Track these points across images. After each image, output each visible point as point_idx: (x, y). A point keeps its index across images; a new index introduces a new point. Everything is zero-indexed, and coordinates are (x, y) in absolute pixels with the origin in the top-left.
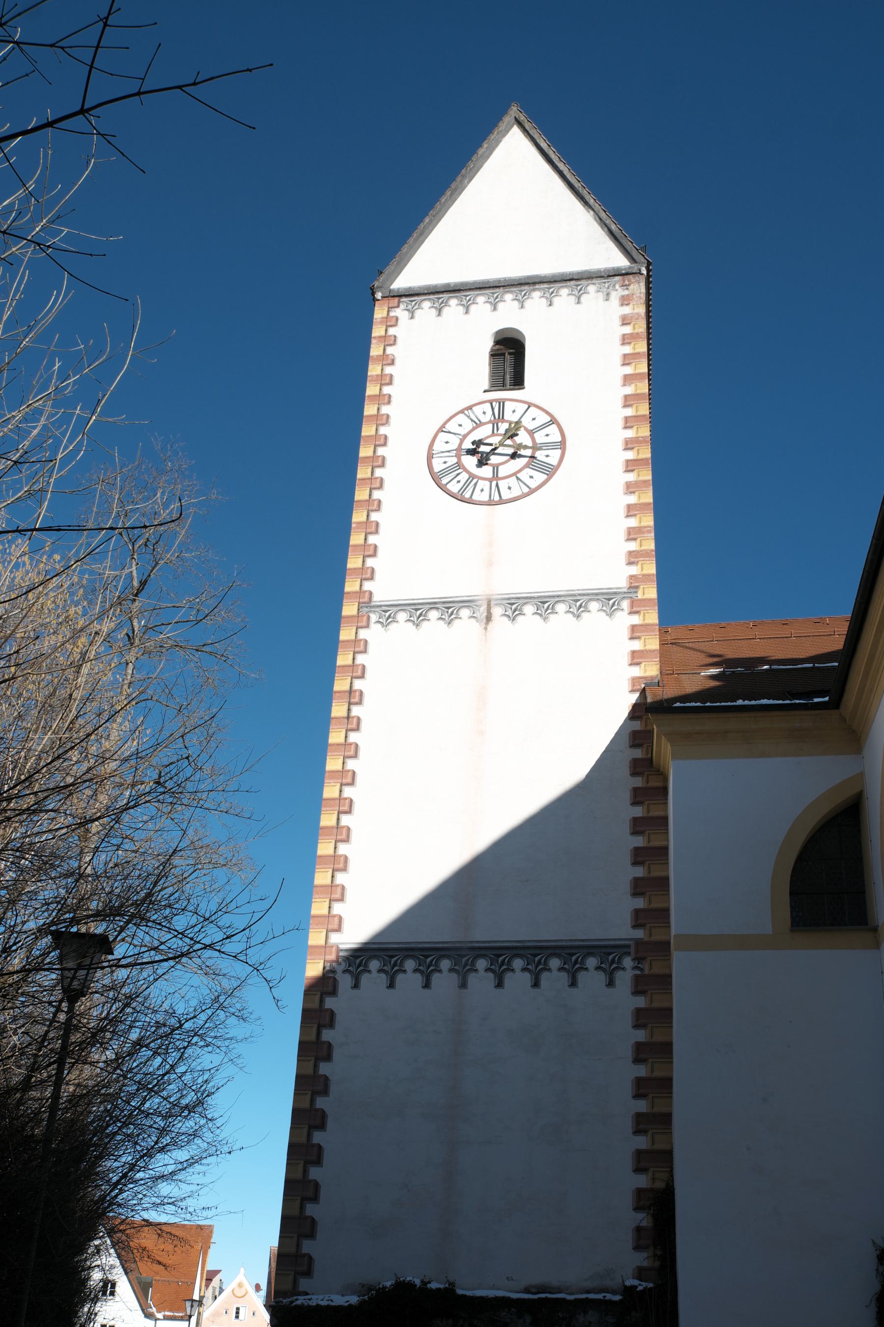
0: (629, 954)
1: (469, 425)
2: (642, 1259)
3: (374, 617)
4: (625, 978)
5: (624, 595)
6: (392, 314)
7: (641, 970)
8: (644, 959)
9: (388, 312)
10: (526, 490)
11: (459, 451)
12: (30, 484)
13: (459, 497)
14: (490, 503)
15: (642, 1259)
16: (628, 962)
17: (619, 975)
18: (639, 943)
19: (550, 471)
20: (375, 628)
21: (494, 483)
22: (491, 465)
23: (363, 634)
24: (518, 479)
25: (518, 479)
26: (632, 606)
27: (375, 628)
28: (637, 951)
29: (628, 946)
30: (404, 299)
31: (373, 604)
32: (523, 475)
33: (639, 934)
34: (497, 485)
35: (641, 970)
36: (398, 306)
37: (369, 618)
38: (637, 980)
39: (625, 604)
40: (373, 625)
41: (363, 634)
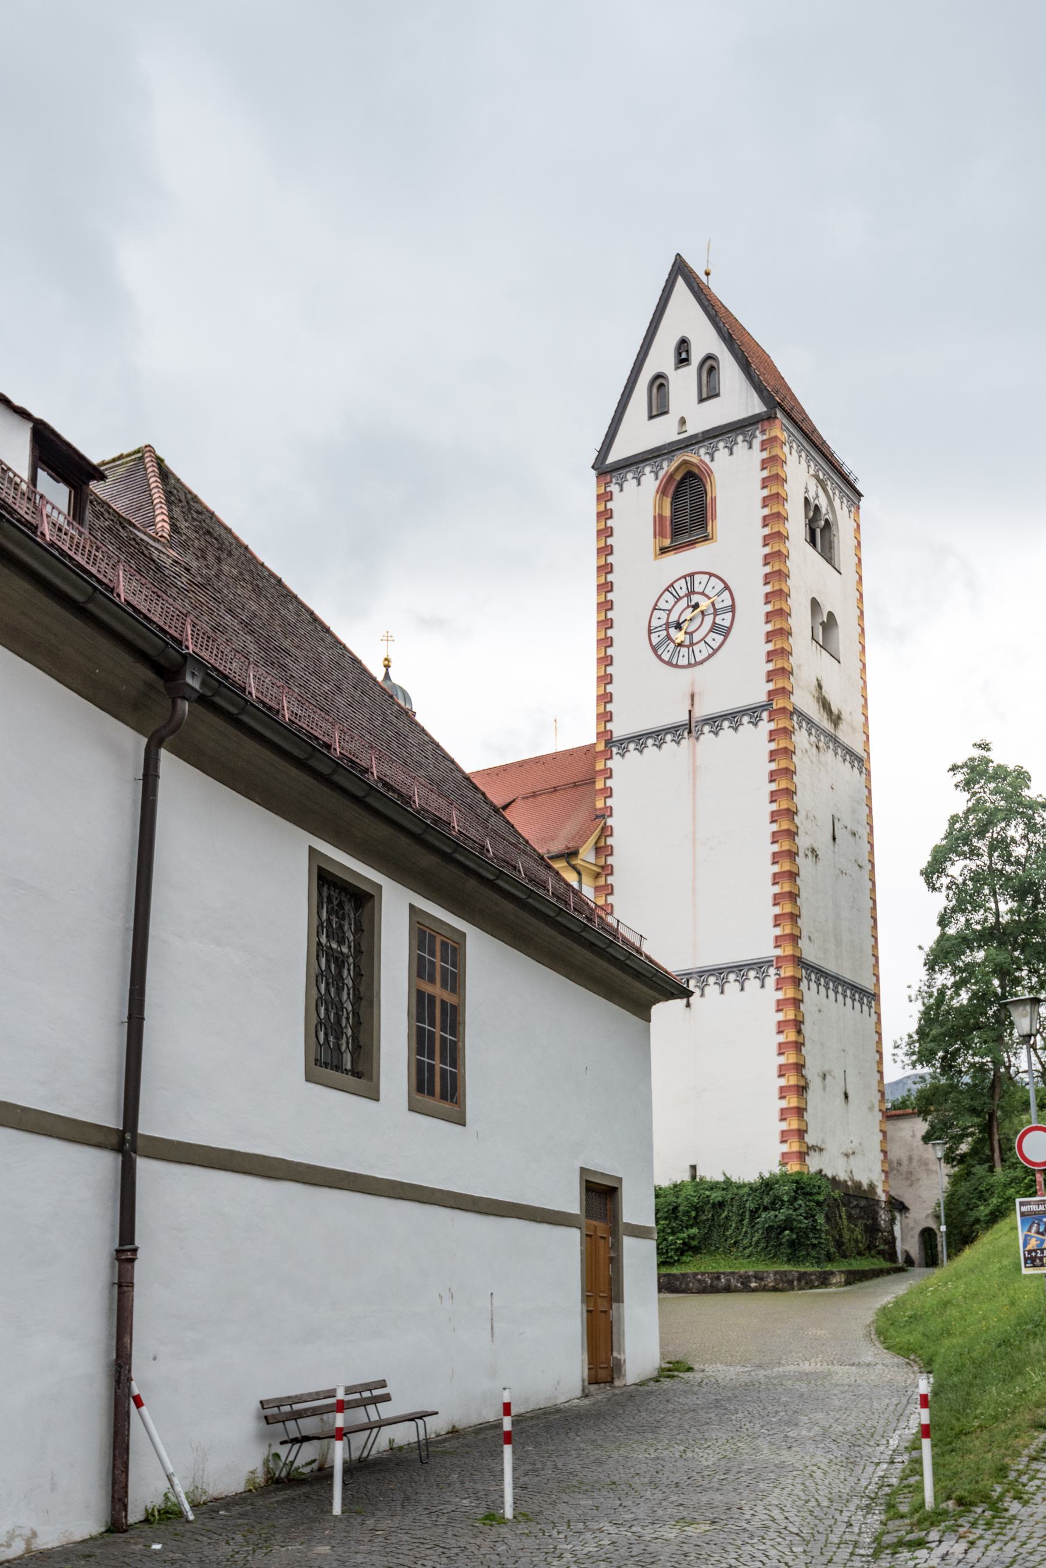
0: (772, 965)
1: (672, 600)
2: (741, 447)
3: (615, 750)
4: (771, 981)
5: (763, 707)
6: (608, 489)
7: (779, 975)
8: (781, 967)
9: (605, 488)
10: (711, 651)
11: (668, 625)
12: (352, 944)
13: (669, 663)
14: (689, 665)
15: (741, 447)
16: (772, 971)
17: (767, 980)
18: (778, 958)
19: (726, 632)
20: (616, 758)
21: (691, 649)
22: (684, 597)
23: (610, 764)
24: (706, 642)
25: (706, 642)
26: (770, 715)
27: (616, 758)
28: (777, 963)
29: (772, 961)
30: (615, 474)
31: (614, 739)
32: (708, 640)
33: (779, 952)
34: (693, 651)
35: (779, 975)
36: (611, 482)
37: (611, 751)
38: (778, 981)
39: (765, 715)
40: (615, 756)
41: (610, 764)
